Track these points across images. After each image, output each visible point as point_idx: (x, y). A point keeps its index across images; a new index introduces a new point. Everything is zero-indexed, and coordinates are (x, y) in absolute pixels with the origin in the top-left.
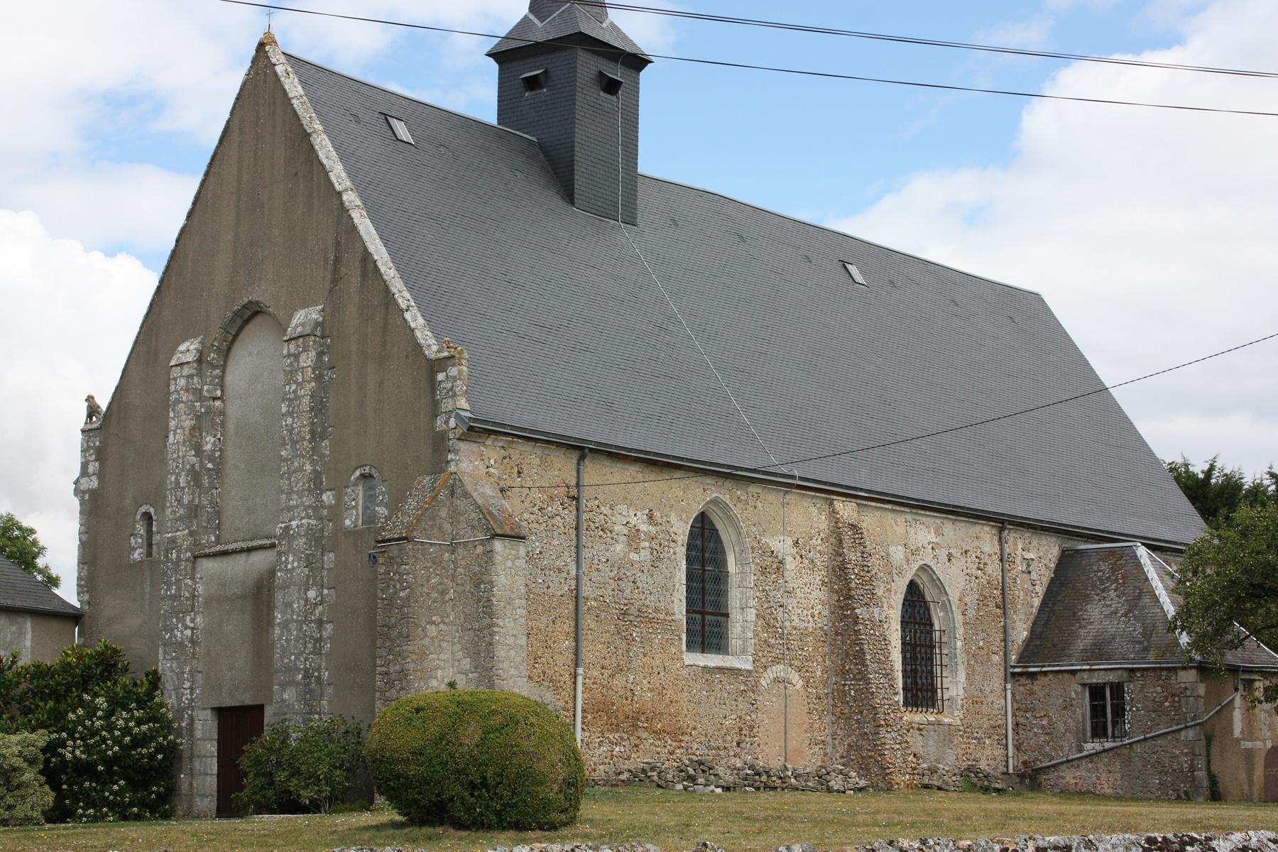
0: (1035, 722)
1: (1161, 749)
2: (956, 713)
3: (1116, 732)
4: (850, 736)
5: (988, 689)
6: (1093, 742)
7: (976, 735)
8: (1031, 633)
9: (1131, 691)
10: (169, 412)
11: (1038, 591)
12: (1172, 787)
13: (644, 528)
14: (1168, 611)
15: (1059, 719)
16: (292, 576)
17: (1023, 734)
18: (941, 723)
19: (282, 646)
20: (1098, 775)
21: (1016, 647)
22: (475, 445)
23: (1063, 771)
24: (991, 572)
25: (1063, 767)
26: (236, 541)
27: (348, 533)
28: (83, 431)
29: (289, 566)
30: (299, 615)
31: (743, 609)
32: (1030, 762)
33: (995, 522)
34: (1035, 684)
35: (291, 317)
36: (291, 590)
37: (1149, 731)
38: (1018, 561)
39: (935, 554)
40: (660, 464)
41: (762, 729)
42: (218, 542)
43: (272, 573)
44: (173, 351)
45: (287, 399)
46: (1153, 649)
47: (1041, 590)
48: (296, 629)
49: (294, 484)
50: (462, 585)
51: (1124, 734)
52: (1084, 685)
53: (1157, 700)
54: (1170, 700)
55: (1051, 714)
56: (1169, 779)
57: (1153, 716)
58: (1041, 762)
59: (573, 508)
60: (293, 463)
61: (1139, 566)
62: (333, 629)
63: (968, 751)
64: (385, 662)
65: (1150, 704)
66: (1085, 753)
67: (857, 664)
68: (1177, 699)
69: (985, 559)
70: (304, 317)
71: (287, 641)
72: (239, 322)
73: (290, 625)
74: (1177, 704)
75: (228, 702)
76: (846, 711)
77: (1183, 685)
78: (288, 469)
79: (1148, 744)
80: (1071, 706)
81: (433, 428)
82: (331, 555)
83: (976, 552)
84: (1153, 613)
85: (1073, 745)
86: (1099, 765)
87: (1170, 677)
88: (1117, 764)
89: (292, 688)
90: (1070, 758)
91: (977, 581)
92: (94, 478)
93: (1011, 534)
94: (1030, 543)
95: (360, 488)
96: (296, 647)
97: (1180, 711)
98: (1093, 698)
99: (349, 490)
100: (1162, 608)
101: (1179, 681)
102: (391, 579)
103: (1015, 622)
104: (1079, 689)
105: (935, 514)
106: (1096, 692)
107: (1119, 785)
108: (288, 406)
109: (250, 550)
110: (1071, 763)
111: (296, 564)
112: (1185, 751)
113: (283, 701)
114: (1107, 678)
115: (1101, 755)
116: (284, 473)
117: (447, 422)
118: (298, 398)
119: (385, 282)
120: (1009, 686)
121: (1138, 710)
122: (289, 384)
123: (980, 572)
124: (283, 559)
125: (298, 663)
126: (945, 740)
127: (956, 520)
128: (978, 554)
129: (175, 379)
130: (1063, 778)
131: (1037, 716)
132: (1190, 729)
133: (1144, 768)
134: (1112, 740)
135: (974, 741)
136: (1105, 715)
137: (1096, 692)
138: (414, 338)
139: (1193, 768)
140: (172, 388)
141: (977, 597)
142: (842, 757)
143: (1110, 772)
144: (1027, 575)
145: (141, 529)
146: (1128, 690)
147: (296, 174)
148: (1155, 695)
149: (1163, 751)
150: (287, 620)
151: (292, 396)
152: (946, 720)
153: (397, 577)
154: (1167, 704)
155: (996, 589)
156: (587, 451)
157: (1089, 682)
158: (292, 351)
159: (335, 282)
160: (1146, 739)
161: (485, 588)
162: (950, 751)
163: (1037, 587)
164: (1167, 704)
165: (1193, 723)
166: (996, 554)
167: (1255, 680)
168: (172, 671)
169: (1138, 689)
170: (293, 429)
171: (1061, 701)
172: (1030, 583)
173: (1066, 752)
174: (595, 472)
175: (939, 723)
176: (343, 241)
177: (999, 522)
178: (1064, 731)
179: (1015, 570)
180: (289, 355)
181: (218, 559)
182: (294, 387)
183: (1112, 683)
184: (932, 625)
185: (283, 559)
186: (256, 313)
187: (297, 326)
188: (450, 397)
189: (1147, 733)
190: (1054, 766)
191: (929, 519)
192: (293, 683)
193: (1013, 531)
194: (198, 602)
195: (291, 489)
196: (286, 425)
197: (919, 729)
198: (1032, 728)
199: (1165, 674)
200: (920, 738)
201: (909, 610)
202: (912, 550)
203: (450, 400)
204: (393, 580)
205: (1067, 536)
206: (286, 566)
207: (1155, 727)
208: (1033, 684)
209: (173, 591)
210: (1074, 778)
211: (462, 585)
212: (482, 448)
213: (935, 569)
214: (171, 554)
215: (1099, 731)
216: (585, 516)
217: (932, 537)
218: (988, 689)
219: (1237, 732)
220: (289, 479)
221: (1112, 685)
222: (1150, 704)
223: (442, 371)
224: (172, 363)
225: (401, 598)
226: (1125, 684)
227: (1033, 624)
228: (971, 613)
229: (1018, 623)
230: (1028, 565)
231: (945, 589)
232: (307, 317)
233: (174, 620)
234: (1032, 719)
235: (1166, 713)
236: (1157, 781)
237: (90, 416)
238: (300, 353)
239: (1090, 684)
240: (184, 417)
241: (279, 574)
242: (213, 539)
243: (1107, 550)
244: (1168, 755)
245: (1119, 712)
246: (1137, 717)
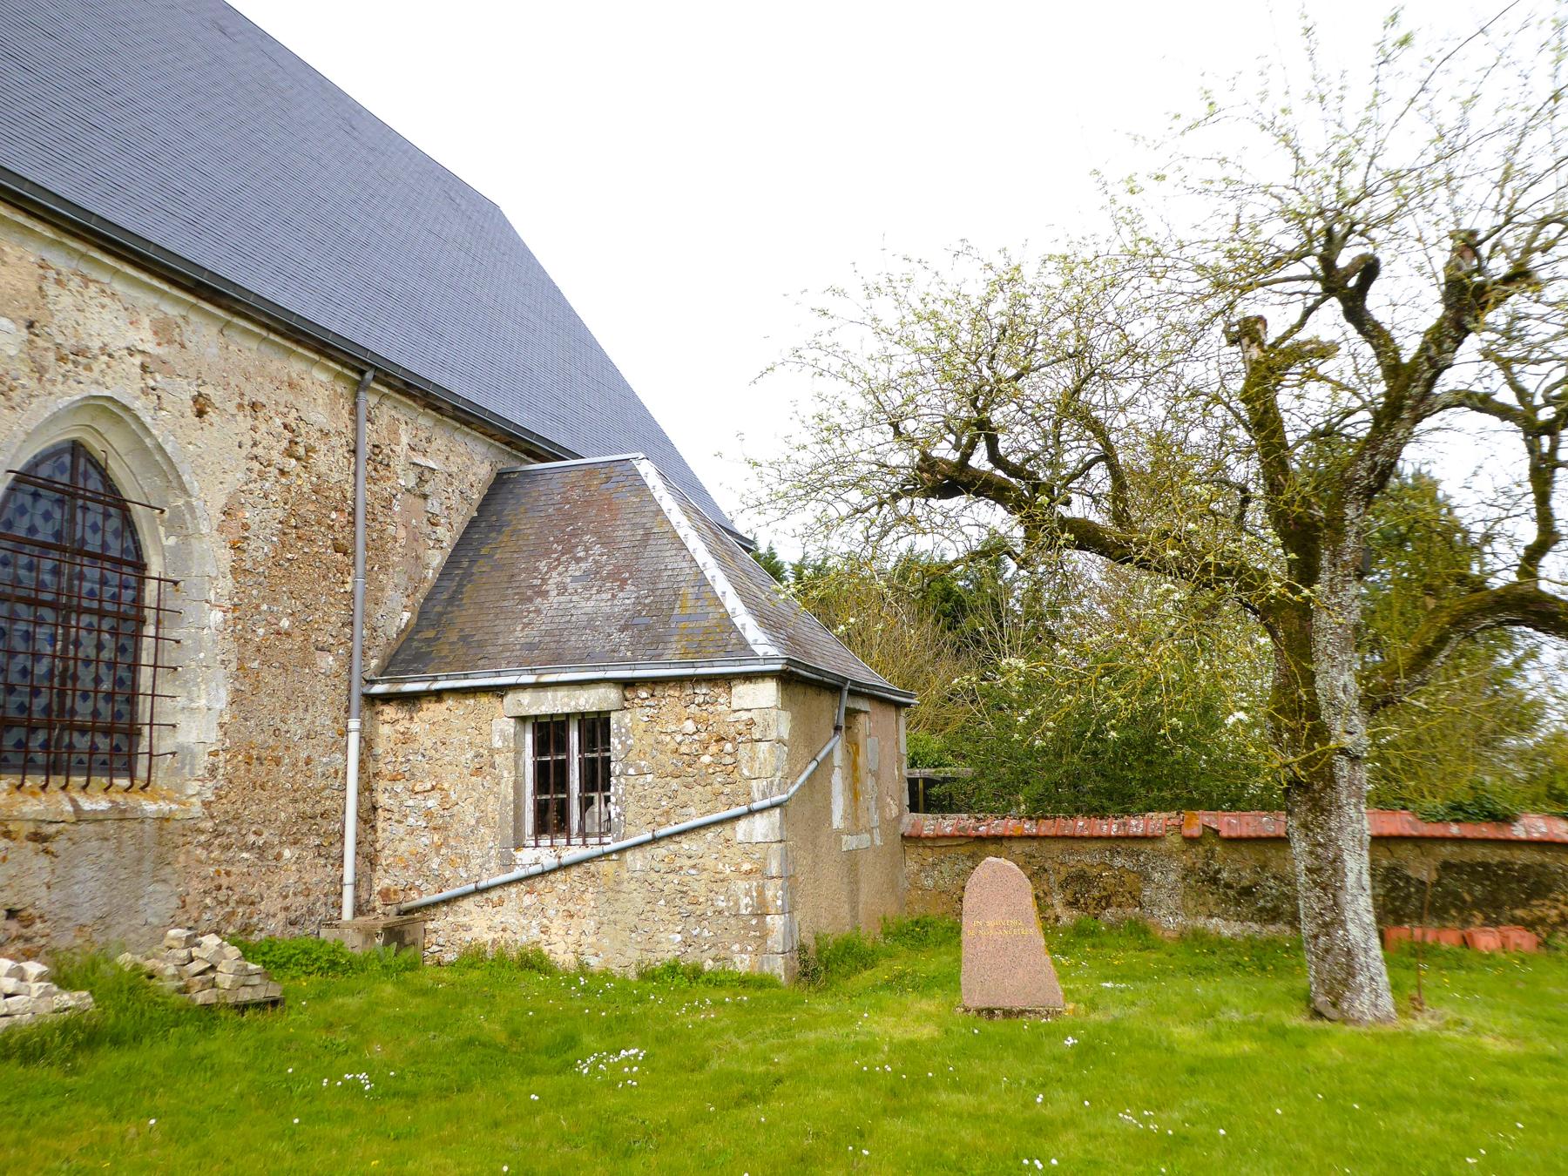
0: (411, 803)
1: (692, 862)
2: (193, 787)
3: (588, 821)
5: (298, 730)
6: (537, 846)
7: (252, 838)
8: (419, 618)
9: (628, 728)
11: (441, 537)
12: (713, 952)
14: (704, 565)
15: (464, 796)
17: (384, 830)
18: (128, 815)
20: (545, 921)
21: (381, 641)
23: (468, 913)
24: (323, 469)
25: (467, 904)
32: (395, 892)
33: (344, 365)
34: (416, 719)
37: (663, 820)
38: (398, 464)
39: (152, 383)
46: (676, 638)
47: (448, 536)
51: (607, 827)
52: (522, 719)
53: (683, 749)
54: (713, 748)
55: (446, 786)
56: (706, 933)
57: (675, 787)
58: (421, 893)
61: (641, 487)
63: (224, 881)
65: (668, 760)
66: (518, 873)
68: (728, 747)
69: (307, 436)
74: (728, 760)
77: (745, 716)
79: (661, 851)
80: (493, 766)
83: (285, 415)
84: (673, 569)
85: (493, 852)
86: (548, 899)
88: (588, 896)
90: (482, 884)
91: (283, 480)
93: (384, 408)
94: (429, 440)
97: (736, 775)
98: (541, 747)
100: (693, 560)
101: (734, 706)
103: (383, 590)
104: (510, 727)
105: (155, 283)
106: (549, 732)
107: (591, 946)
110: (486, 895)
112: (746, 867)
114: (573, 703)
115: (551, 877)
120: (354, 724)
123: (293, 461)
126: (140, 860)
127: (228, 323)
128: (291, 420)
130: (468, 929)
131: (417, 789)
132: (757, 816)
133: (648, 907)
134: (579, 841)
135: (245, 855)
136: (563, 785)
137: (549, 732)
139: (761, 912)
141: (280, 515)
143: (572, 916)
144: (421, 501)
146: (619, 728)
148: (679, 738)
149: (694, 867)
152: (150, 807)
154: (706, 759)
155: (336, 509)
157: (534, 711)
160: (655, 840)
162: (159, 887)
163: (440, 530)
165: (767, 802)
166: (340, 433)
167: (859, 711)
169: (642, 726)
171: (470, 755)
172: (425, 521)
173: (476, 870)
175: (122, 816)
177: (353, 369)
178: (473, 822)
179: (390, 483)
183: (583, 714)
184: (140, 566)
189: (659, 825)
190: (447, 902)
191: (135, 293)
193: (388, 403)
197: (36, 837)
198: (406, 816)
199: (704, 691)
200: (44, 861)
201: (57, 514)
202: (58, 346)
205: (509, 449)
207: (679, 811)
208: (411, 718)
210: (489, 928)
213: (147, 420)
215: (551, 820)
217: (144, 337)
218: (298, 730)
219: (837, 821)
221: (582, 717)
222: (668, 760)
226: (614, 716)
227: (427, 599)
228: (260, 550)
229: (389, 592)
230: (421, 480)
231: (179, 477)
234: (404, 796)
235: (704, 780)
236: (679, 937)
239: (536, 717)
243: (584, 468)
244: (705, 875)
245: (597, 777)
246: (639, 789)
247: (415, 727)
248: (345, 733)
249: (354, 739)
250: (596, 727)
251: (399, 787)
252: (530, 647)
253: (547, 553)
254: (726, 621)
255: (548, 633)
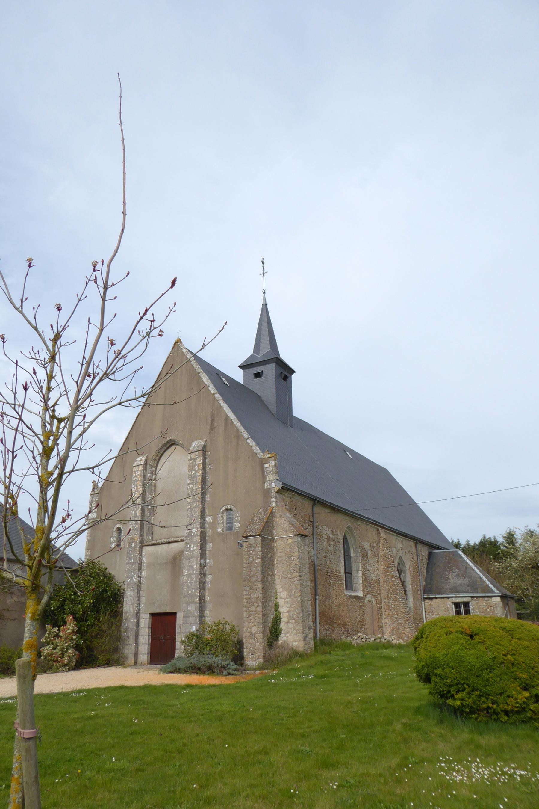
4: (393, 624)
10: (132, 485)
13: (331, 536)
16: (193, 553)
19: (188, 585)
22: (282, 495)
26: (161, 539)
27: (219, 534)
28: (91, 495)
29: (192, 549)
30: (196, 571)
31: (357, 571)
35: (191, 444)
36: (192, 560)
40: (336, 509)
41: (367, 622)
42: (152, 539)
43: (182, 552)
44: (134, 461)
45: (190, 477)
48: (195, 577)
49: (193, 513)
50: (281, 557)
52: (452, 603)
59: (311, 526)
60: (193, 504)
62: (212, 578)
64: (248, 593)
67: (394, 594)
70: (196, 444)
71: (190, 583)
72: (164, 448)
73: (192, 576)
75: (158, 611)
76: (391, 614)
77: (495, 603)
78: (191, 507)
81: (263, 487)
82: (211, 544)
87: (489, 600)
89: (193, 605)
92: (95, 514)
95: (225, 515)
96: (195, 586)
99: (220, 516)
102: (251, 554)
104: (451, 604)
106: (457, 605)
108: (191, 480)
109: (169, 543)
111: (195, 548)
113: (188, 610)
116: (189, 509)
117: (270, 485)
118: (195, 476)
119: (237, 428)
121: (476, 612)
122: (191, 471)
124: (189, 546)
125: (196, 593)
129: (135, 472)
137: (457, 605)
138: (252, 450)
140: (134, 475)
142: (390, 633)
145: (115, 534)
147: (192, 388)
150: (190, 573)
151: (193, 476)
153: (254, 553)
156: (316, 501)
158: (193, 457)
159: (212, 429)
161: (294, 558)
164: (488, 610)
168: (131, 596)
170: (194, 490)
171: (444, 608)
174: (318, 509)
176: (215, 413)
180: (191, 459)
181: (154, 547)
182: (193, 472)
185: (189, 546)
186: (172, 445)
187: (194, 447)
188: (271, 474)
192: (193, 602)
194: (144, 565)
195: (192, 515)
196: (190, 488)
203: (271, 475)
204: (252, 554)
206: (190, 549)
209: (132, 561)
211: (281, 557)
212: (284, 497)
214: (132, 544)
216: (315, 529)
220: (191, 511)
223: (267, 463)
224: (134, 465)
225: (256, 563)
232: (199, 443)
233: (133, 573)
237: (94, 489)
238: (196, 458)
240: (139, 487)
241: (186, 553)
242: (150, 538)
247: (432, 603)
248: (422, 604)
249: (423, 606)
250: (466, 604)
251: (430, 614)
252: (451, 589)
253: (447, 571)
254: (487, 586)
255: (454, 587)
